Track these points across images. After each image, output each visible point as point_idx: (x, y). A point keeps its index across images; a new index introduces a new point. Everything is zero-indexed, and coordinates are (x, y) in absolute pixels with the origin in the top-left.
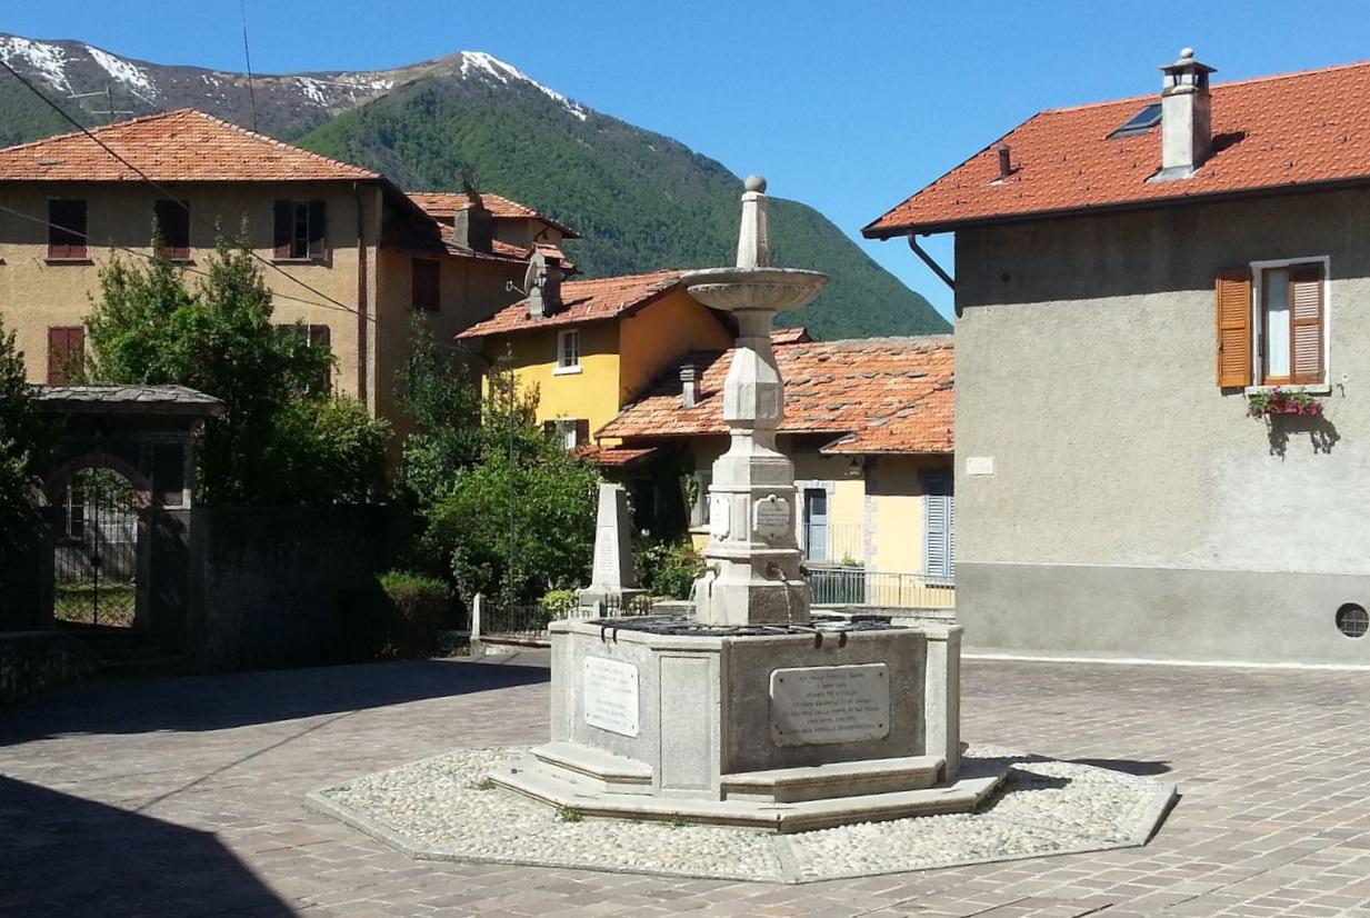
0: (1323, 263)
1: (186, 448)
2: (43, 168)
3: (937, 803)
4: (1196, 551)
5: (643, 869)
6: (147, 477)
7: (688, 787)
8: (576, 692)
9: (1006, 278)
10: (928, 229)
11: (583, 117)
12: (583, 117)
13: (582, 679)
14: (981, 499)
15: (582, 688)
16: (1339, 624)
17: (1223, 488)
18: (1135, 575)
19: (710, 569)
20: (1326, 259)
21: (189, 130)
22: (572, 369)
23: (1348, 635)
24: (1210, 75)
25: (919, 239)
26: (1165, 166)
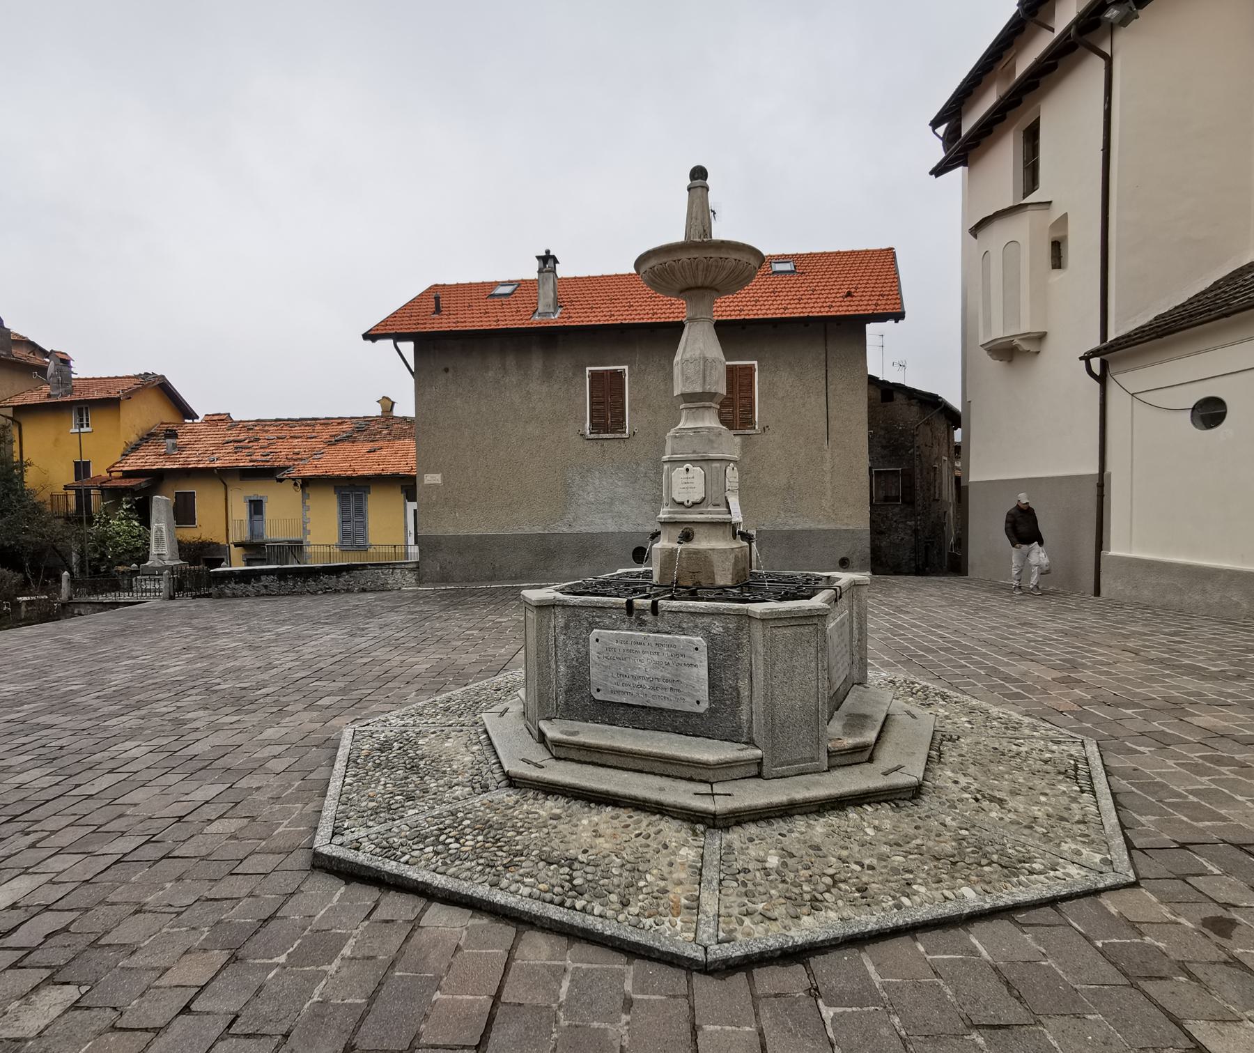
9: (447, 370)
14: (434, 498)
20: (626, 367)
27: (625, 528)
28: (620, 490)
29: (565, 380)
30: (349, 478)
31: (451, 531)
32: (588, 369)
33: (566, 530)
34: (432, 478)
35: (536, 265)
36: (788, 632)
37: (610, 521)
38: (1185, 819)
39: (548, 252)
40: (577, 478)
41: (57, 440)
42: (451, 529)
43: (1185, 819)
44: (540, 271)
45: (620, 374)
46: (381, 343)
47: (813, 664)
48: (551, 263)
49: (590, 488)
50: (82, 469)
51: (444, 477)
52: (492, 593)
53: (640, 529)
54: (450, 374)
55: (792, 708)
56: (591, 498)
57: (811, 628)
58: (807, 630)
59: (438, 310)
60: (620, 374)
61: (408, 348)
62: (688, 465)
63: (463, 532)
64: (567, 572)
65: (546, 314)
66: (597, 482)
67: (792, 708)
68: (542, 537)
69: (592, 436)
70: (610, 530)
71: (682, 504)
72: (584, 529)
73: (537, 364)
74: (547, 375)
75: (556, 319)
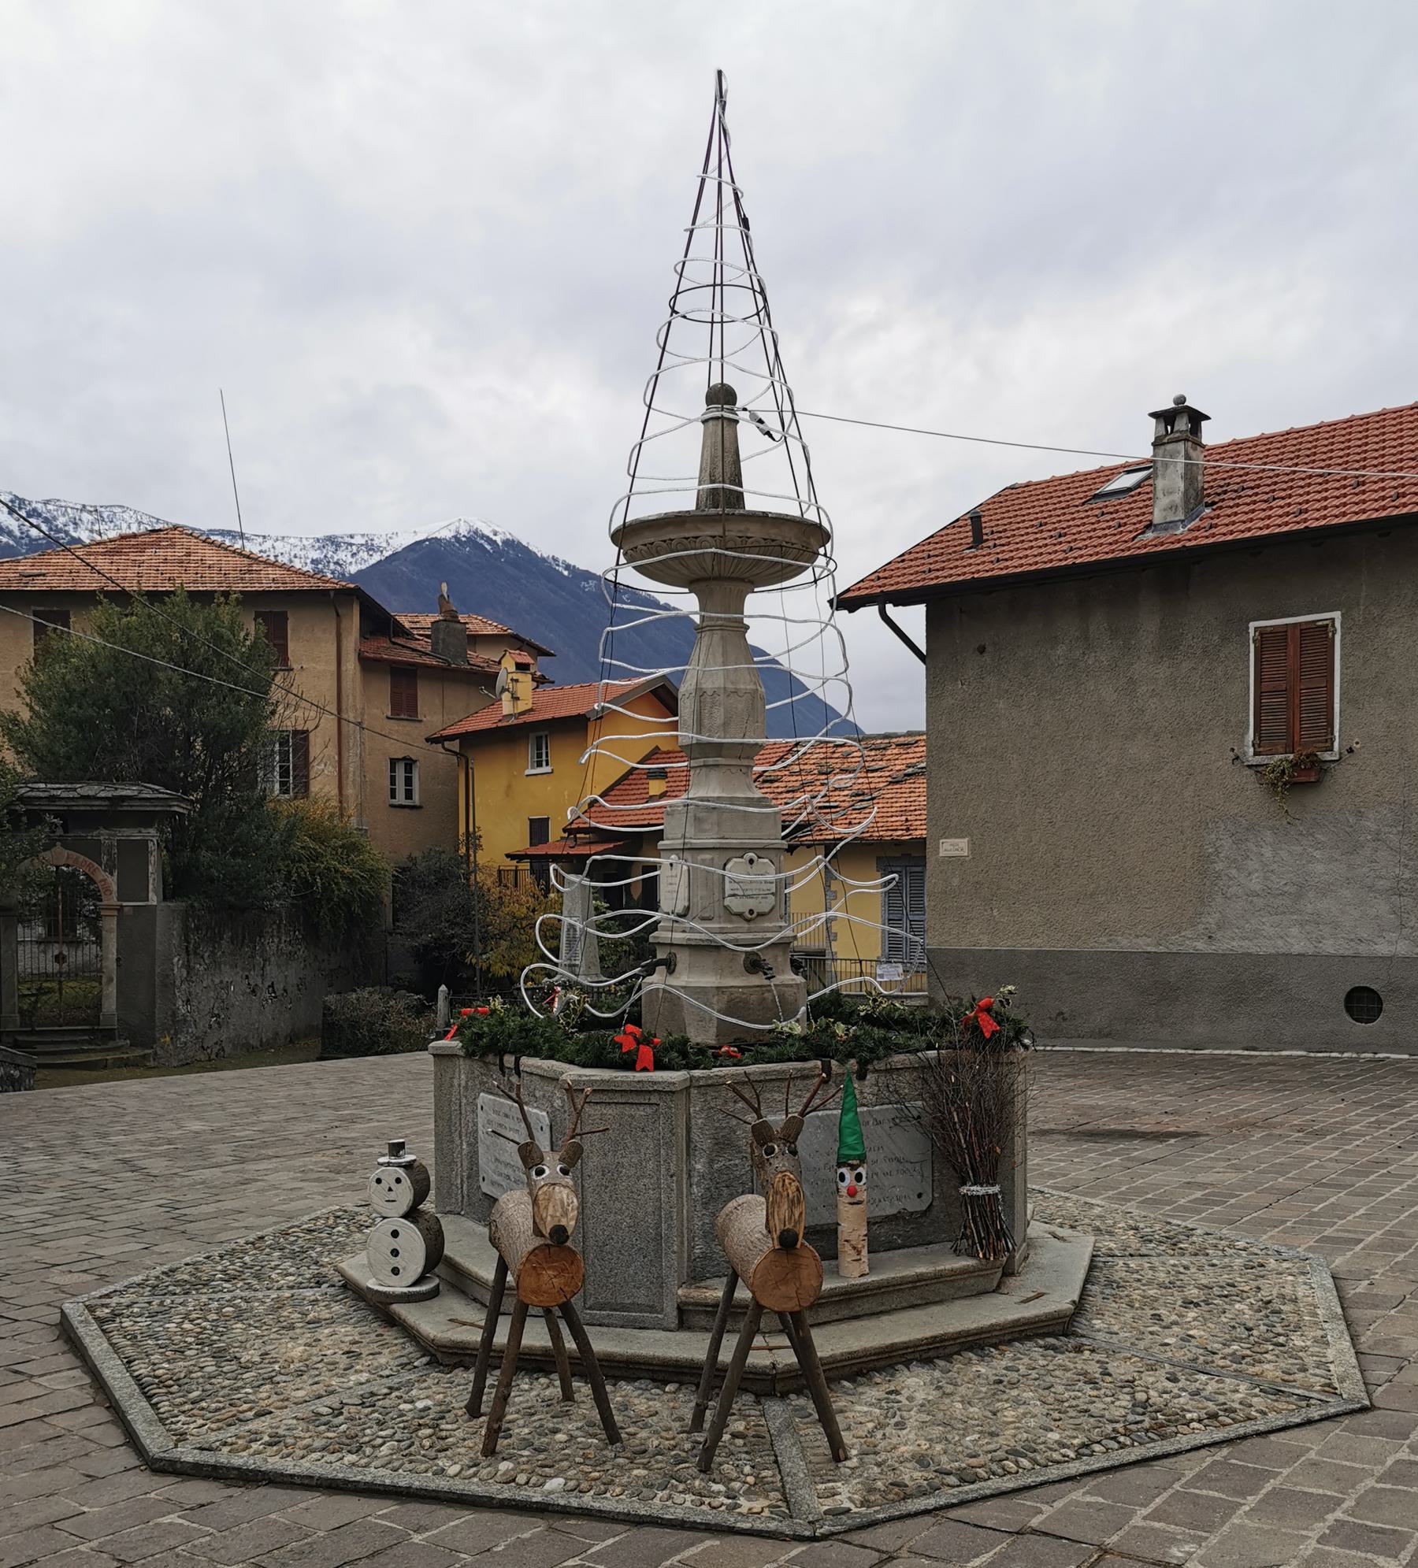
0: (1333, 620)
1: (150, 844)
2: (25, 580)
3: (1016, 1323)
4: (1188, 933)
5: (537, 1498)
6: (111, 874)
7: (623, 1308)
8: (469, 1145)
9: (982, 650)
10: (904, 598)
11: (566, 573)
12: (566, 573)
13: (475, 1124)
14: (956, 882)
15: (476, 1139)
16: (1349, 1010)
17: (1219, 866)
18: (1125, 957)
19: (661, 962)
20: (1337, 615)
21: (173, 546)
22: (545, 769)
23: (1357, 1020)
24: (1204, 423)
25: (889, 607)
26: (1155, 522)
27: (1329, 947)
28: (1320, 868)
29: (1205, 651)
30: (897, 843)
31: (985, 944)
32: (1252, 625)
33: (1201, 946)
34: (953, 847)
35: (1150, 429)
36: (609, 1111)
37: (1295, 931)
38: (1216, 1494)
39: (1181, 400)
40: (1227, 843)
41: (509, 787)
42: (985, 939)
43: (1216, 1494)
44: (1157, 444)
45: (1323, 632)
46: (863, 612)
47: (651, 1165)
48: (1182, 424)
49: (1252, 865)
50: (538, 829)
51: (973, 845)
52: (1108, 1060)
53: (1363, 949)
54: (987, 657)
55: (617, 1226)
56: (1255, 884)
57: (649, 1110)
58: (640, 1112)
59: (978, 540)
60: (1323, 632)
61: (913, 618)
62: (751, 855)
63: (1003, 947)
64: (1200, 1029)
65: (1168, 525)
66: (1268, 852)
67: (617, 1226)
68: (1153, 958)
69: (1259, 760)
70: (1297, 949)
71: (740, 915)
72: (1238, 945)
73: (1149, 626)
74: (1169, 645)
75: (1184, 535)
